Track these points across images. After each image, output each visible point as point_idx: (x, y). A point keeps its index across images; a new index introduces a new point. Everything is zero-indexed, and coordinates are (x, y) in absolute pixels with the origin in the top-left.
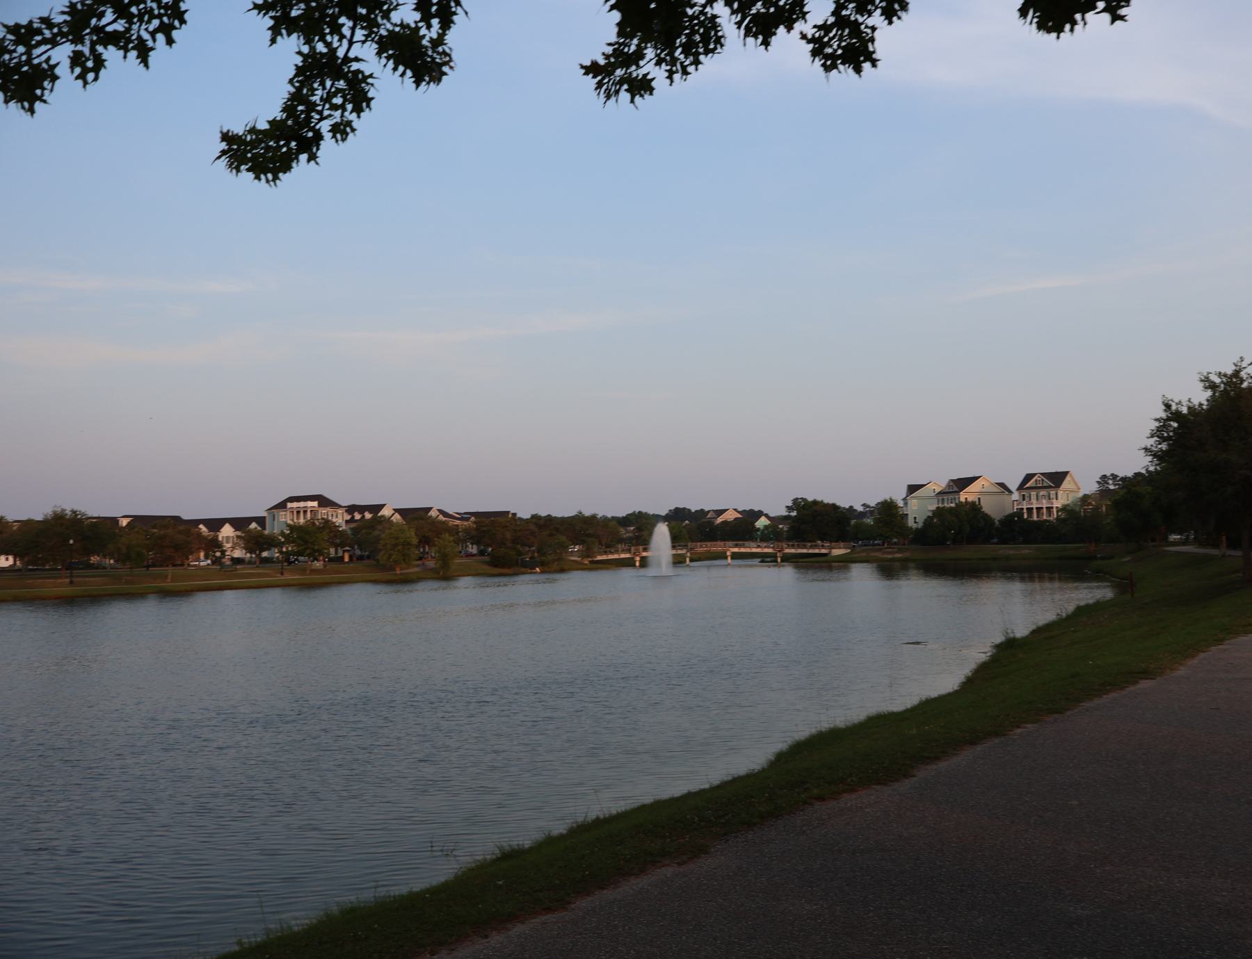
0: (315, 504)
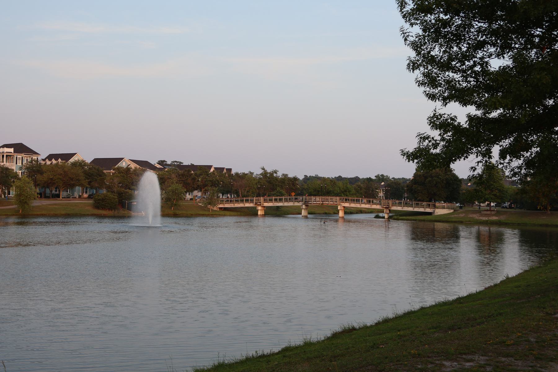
0: (12, 150)
